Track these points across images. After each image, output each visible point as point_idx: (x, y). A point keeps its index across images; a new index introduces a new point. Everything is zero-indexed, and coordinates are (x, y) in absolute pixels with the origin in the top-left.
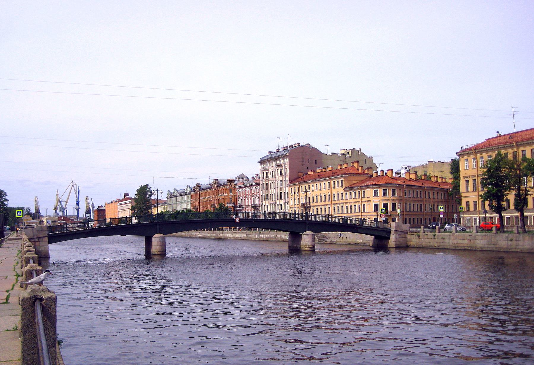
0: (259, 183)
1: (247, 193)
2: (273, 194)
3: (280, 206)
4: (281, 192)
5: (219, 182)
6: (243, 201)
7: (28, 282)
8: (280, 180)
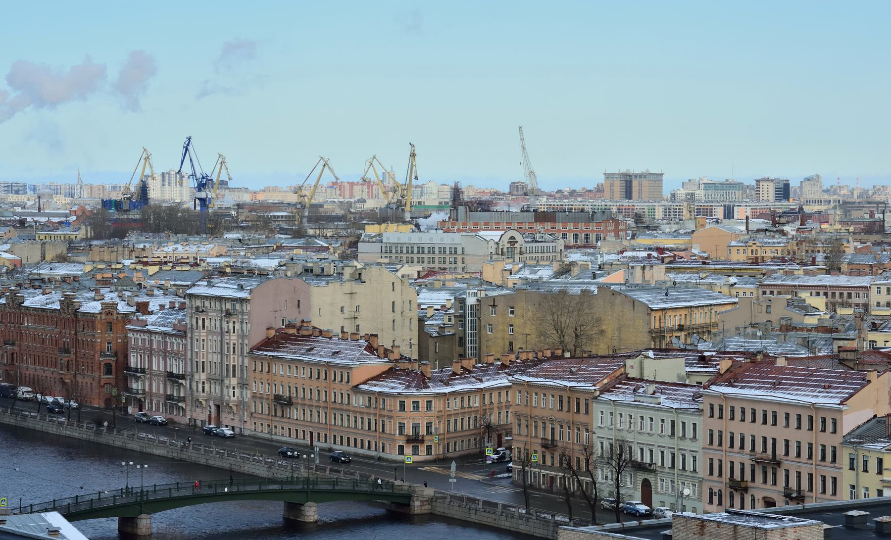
1: (155, 346)
3: (231, 391)
4: (234, 364)
6: (144, 361)
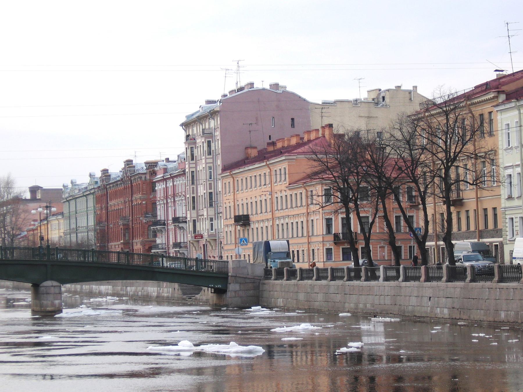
0: (184, 171)
2: (202, 195)
5: (134, 167)
7: (455, 265)
8: (208, 165)
